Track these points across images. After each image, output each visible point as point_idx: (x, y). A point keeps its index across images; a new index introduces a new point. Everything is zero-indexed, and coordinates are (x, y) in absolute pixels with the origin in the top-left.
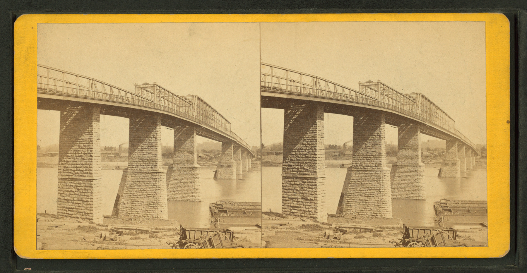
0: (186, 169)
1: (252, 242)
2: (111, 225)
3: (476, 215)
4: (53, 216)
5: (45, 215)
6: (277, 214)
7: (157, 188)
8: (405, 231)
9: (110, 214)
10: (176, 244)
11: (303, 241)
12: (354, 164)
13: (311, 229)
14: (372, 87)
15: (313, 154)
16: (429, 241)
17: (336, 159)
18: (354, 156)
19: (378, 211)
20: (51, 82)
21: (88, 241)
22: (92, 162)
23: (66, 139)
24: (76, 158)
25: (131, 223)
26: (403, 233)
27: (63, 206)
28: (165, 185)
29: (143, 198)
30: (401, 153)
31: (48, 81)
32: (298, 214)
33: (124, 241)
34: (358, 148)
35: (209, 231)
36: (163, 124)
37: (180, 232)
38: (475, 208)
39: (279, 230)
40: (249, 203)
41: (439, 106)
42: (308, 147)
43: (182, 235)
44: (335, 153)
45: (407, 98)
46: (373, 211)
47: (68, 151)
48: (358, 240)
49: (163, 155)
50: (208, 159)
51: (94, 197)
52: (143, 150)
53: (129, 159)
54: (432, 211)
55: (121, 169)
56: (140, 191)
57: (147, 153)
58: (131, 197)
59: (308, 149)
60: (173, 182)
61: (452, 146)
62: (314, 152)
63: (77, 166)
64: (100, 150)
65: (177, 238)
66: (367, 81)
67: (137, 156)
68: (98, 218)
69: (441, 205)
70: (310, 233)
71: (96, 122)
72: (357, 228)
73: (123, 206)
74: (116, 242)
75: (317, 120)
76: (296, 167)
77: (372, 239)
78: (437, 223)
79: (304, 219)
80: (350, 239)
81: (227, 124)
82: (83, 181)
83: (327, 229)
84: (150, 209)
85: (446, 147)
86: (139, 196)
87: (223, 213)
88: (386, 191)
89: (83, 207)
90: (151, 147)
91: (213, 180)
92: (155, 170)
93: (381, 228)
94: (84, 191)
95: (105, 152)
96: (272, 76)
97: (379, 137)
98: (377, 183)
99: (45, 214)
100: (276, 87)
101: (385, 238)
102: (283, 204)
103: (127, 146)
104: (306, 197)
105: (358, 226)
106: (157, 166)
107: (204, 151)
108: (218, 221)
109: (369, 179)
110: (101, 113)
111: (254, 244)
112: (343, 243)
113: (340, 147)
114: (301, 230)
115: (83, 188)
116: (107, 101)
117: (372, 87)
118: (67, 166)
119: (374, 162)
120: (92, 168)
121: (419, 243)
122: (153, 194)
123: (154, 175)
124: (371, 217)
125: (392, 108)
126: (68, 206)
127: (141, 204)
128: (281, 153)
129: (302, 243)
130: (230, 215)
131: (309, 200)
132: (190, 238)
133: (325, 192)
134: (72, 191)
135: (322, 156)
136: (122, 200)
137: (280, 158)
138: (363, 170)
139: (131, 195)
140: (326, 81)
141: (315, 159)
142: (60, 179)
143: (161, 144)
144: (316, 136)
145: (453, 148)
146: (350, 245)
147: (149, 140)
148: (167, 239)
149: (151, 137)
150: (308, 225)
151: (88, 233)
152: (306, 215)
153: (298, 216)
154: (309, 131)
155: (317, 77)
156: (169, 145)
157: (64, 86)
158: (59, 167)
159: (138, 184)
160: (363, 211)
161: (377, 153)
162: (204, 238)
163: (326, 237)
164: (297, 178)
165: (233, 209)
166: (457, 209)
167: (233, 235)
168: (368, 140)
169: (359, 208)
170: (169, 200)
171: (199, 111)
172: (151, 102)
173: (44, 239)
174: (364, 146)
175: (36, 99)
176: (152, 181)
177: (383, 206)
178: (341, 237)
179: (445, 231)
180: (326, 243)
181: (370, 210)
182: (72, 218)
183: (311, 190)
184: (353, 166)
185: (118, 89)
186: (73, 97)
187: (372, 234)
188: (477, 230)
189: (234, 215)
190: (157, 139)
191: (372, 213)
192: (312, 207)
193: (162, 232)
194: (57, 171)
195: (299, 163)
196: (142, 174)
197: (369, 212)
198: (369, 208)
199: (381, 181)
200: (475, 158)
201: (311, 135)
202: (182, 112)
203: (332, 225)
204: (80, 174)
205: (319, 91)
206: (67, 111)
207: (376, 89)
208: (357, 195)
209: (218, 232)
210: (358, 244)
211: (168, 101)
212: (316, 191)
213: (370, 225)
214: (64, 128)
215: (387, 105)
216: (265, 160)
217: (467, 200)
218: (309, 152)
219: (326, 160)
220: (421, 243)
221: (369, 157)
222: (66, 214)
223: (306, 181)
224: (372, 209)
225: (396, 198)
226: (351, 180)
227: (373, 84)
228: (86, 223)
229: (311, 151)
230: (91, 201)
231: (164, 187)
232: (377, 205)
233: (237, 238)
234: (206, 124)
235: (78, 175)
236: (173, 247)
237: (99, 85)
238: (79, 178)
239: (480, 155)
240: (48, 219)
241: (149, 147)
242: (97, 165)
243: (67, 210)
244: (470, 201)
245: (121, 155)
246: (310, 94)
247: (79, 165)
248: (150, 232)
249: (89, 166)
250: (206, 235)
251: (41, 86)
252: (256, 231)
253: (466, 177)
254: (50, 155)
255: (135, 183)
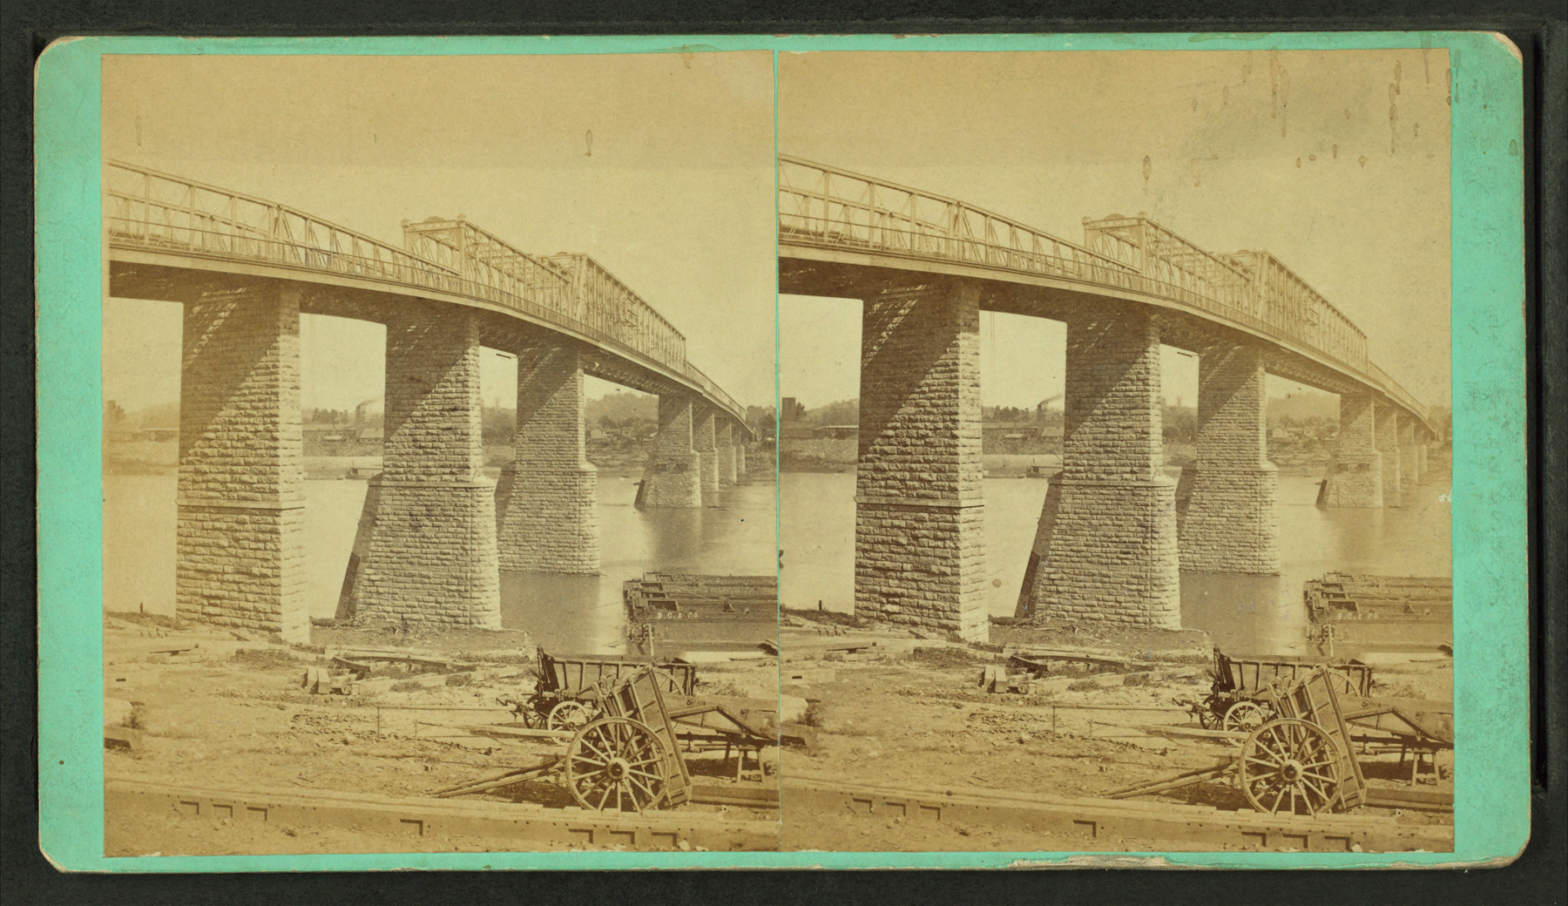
0: (553, 478)
1: (1428, 697)
2: (335, 646)
3: (1428, 622)
4: (163, 621)
5: (141, 616)
6: (841, 618)
7: (469, 536)
8: (543, 668)
9: (330, 613)
10: (1201, 703)
11: (919, 699)
12: (1068, 465)
13: (940, 663)
14: (1122, 234)
15: (948, 435)
16: (1291, 698)
17: (1014, 451)
18: (387, 444)
19: (1139, 608)
20: (156, 215)
21: (267, 695)
22: (277, 456)
23: (199, 387)
24: (229, 444)
25: (1073, 641)
26: (1212, 675)
27: (192, 590)
28: (492, 525)
29: (426, 565)
30: (1208, 433)
31: (147, 212)
32: (902, 616)
33: (1050, 694)
34: (402, 420)
35: (623, 665)
36: (484, 343)
37: (537, 667)
38: (744, 599)
39: (848, 665)
40: (740, 578)
41: (638, 293)
42: (933, 414)
43: (544, 678)
44: (330, 434)
45: (1224, 266)
46: (1125, 608)
47: (887, 421)
48: (1081, 694)
49: (487, 435)
50: (618, 447)
51: (282, 564)
52: (1107, 418)
53: (1065, 446)
54: (1298, 611)
55: (363, 478)
56: (1099, 544)
57: (438, 428)
58: (392, 562)
59: (934, 422)
60: (514, 515)
61: (1359, 413)
62: (951, 429)
63: (234, 468)
64: (300, 420)
65: (529, 686)
66: (427, 217)
67: (1091, 437)
68: (295, 627)
69: (1327, 590)
70: (939, 674)
71: (288, 337)
72: (1079, 660)
73: (369, 589)
74: (350, 697)
75: (959, 332)
76: (898, 475)
77: (1122, 694)
78: (1314, 646)
79: (921, 633)
80: (1057, 693)
81: (676, 341)
82: (251, 514)
83: (987, 661)
84: (1129, 599)
85: (1342, 415)
86: (1095, 559)
87: (1345, 610)
88: (1162, 546)
89: (252, 592)
90: (1129, 409)
91: (635, 510)
92: (462, 481)
93: (1146, 659)
94: (254, 545)
95: (314, 427)
96: (827, 199)
97: (1144, 385)
98: (1135, 523)
99: (139, 615)
100: (838, 233)
101: (481, 690)
102: (858, 588)
103: (378, 407)
104: (928, 564)
105: (402, 652)
106: (1149, 466)
107: (606, 422)
108: (651, 633)
109: (1113, 512)
110: (304, 308)
111: (758, 702)
112: (360, 705)
113: (1025, 415)
114: (913, 666)
115: (931, 533)
116: (1022, 273)
117: (1122, 234)
118: (205, 468)
119: (1127, 458)
120: (277, 474)
121: (1259, 705)
122: (456, 552)
123: (459, 496)
124: (1119, 628)
125: (1182, 295)
126: (206, 592)
127: (1102, 582)
128: (853, 433)
129: (915, 706)
130: (1364, 616)
131: (934, 574)
132: (566, 687)
133: (303, 552)
134: (898, 544)
135: (973, 441)
136: (366, 572)
137: (851, 449)
138: (1094, 483)
139: (391, 555)
140: (985, 216)
141: (952, 449)
142: (185, 509)
143: (1161, 401)
144: (955, 381)
145: (1361, 418)
146: (1057, 710)
147: (443, 390)
148: (500, 689)
149: (1132, 381)
150: (932, 650)
151: (265, 671)
152: (246, 622)
153: (904, 623)
154: (254, 369)
155: (958, 203)
156: (502, 405)
157: (875, 223)
158: (180, 472)
159: (1093, 522)
160: (415, 610)
161: (455, 434)
162: (610, 686)
163: (309, 688)
164: (899, 507)
165: (1373, 598)
166: (692, 603)
167: (693, 674)
168: (1110, 394)
169: (404, 599)
170: (503, 571)
171: (591, 301)
172: (449, 274)
173: (138, 689)
174: (419, 414)
175: (107, 268)
176: (1136, 513)
177: (1154, 594)
178: (1031, 685)
179: (660, 667)
180: (984, 706)
181: (433, 604)
182: (218, 627)
183: (940, 544)
184: (1065, 471)
185: (1033, 233)
186: (904, 257)
187: (1122, 676)
188: (753, 665)
189: (1376, 616)
190: (467, 387)
191: (441, 615)
192: (263, 597)
193: (483, 668)
194: (175, 483)
195: (906, 461)
196: (1104, 491)
197: (433, 611)
198: (1112, 598)
199: (468, 519)
200: (1425, 447)
201: (264, 380)
202: (1222, 302)
203: (1002, 652)
204: (243, 494)
205: (287, 248)
206: (882, 301)
207: (1135, 241)
208: (1077, 559)
209: (650, 666)
210: (1078, 708)
211: (500, 271)
212: (278, 550)
213: (1116, 652)
214: (194, 353)
215: (486, 291)
216: (806, 454)
217: (723, 575)
218: (936, 429)
219: (305, 455)
220: (1265, 705)
221: (1113, 446)
222: (201, 616)
223: (926, 515)
224: (1120, 603)
225: (513, 569)
226: (1059, 515)
227: (1126, 223)
228: (259, 643)
229: (941, 425)
230: (953, 574)
231: (489, 530)
232: (457, 591)
233: (705, 684)
234: (1292, 340)
235: (235, 495)
236: (518, 714)
237: (297, 225)
238: (917, 503)
239: (1441, 439)
240: (150, 629)
241: (443, 410)
242: (291, 467)
243: (205, 602)
244: (1411, 578)
245: (363, 436)
246: (937, 254)
247: (920, 462)
248: (448, 667)
249: (269, 471)
250: (614, 677)
251: (127, 227)
252: (761, 662)
253: (722, 506)
254: (834, 435)
255: (405, 520)
